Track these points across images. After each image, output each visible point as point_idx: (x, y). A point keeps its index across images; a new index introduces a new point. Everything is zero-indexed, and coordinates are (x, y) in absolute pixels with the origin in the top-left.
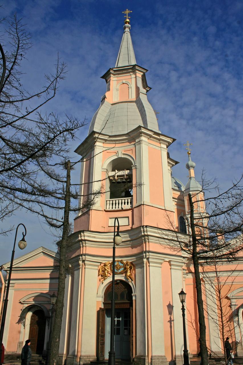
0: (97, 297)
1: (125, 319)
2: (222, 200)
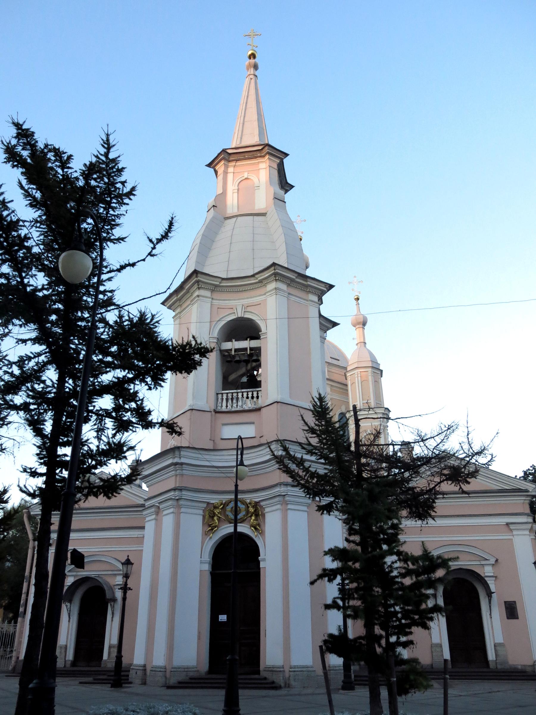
0: (201, 562)
2: (400, 425)
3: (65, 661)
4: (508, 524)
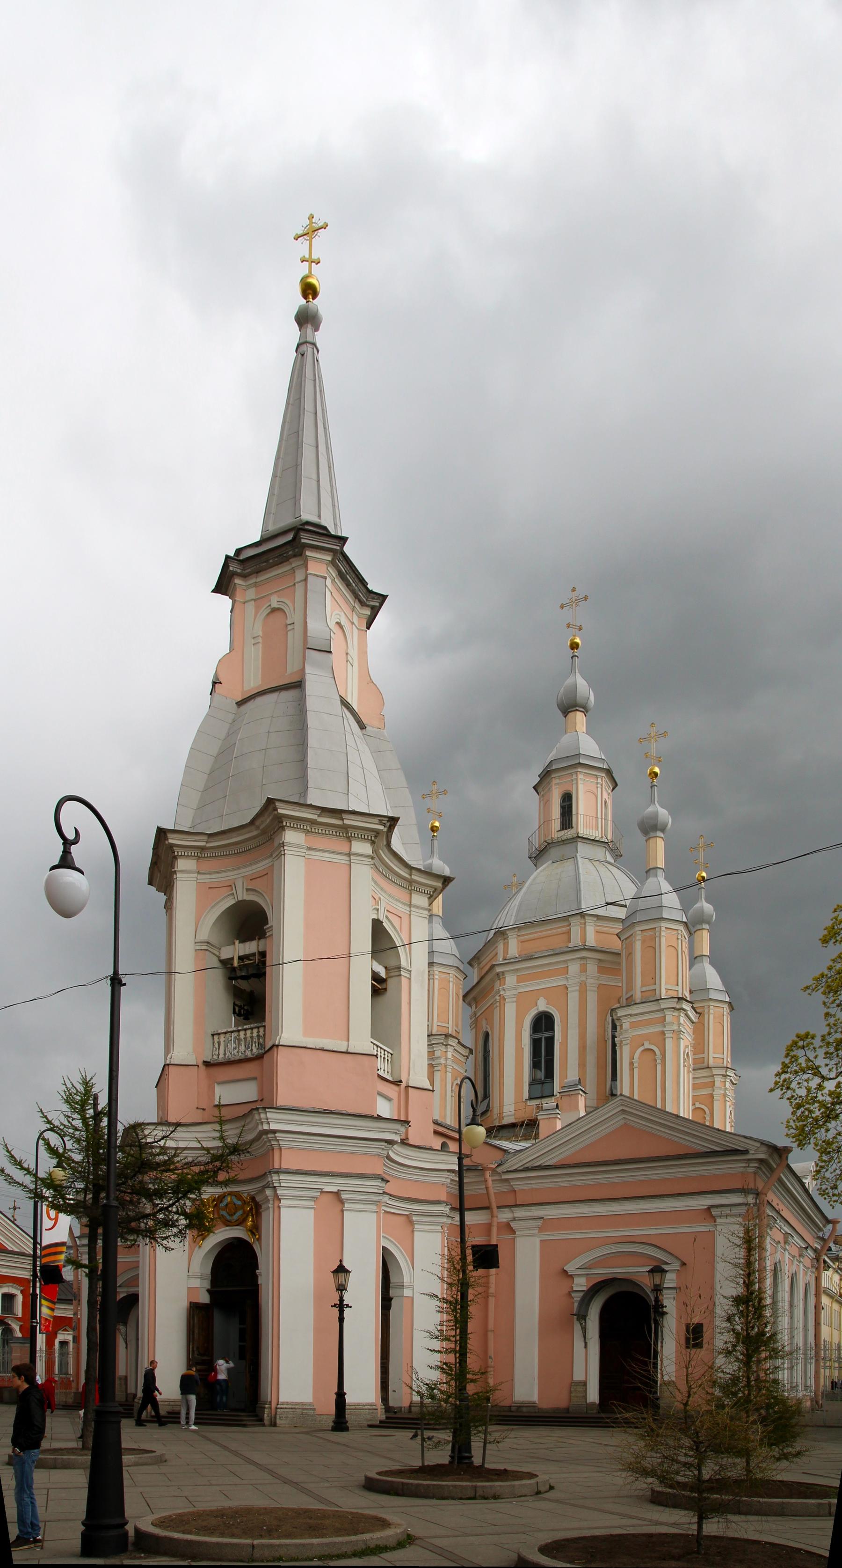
0: (189, 1277)
1: (242, 1326)
3: (127, 1394)
4: (709, 1208)
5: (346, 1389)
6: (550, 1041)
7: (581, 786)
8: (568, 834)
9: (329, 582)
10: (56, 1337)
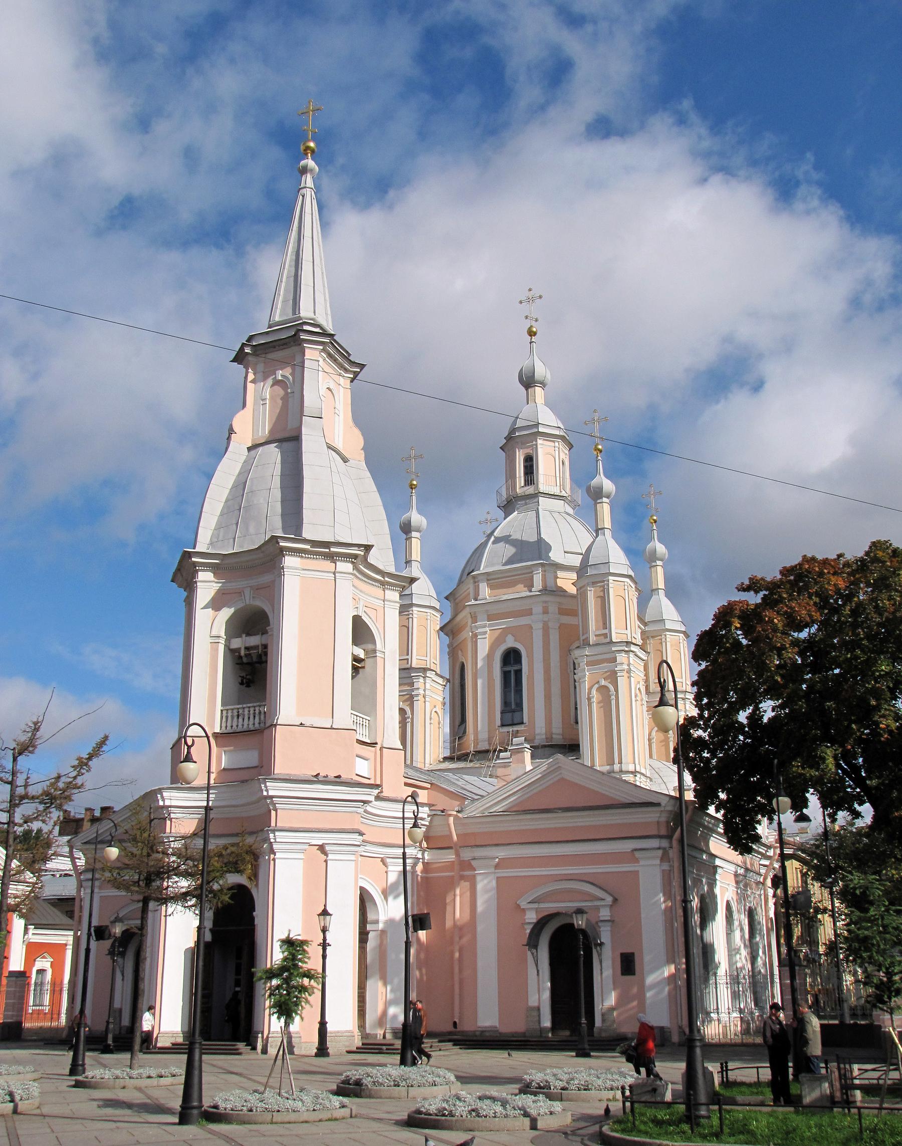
5: (327, 1019)
6: (519, 673)
7: (540, 450)
8: (530, 490)
9: (321, 362)
10: (34, 965)
